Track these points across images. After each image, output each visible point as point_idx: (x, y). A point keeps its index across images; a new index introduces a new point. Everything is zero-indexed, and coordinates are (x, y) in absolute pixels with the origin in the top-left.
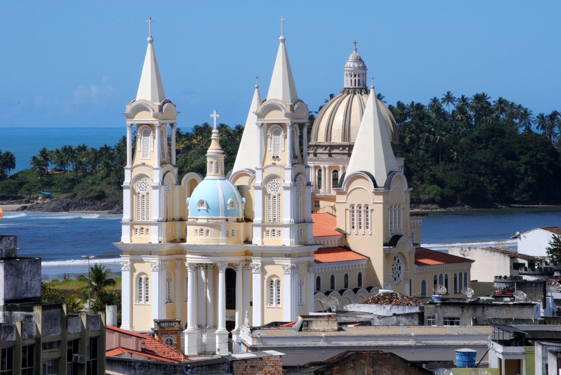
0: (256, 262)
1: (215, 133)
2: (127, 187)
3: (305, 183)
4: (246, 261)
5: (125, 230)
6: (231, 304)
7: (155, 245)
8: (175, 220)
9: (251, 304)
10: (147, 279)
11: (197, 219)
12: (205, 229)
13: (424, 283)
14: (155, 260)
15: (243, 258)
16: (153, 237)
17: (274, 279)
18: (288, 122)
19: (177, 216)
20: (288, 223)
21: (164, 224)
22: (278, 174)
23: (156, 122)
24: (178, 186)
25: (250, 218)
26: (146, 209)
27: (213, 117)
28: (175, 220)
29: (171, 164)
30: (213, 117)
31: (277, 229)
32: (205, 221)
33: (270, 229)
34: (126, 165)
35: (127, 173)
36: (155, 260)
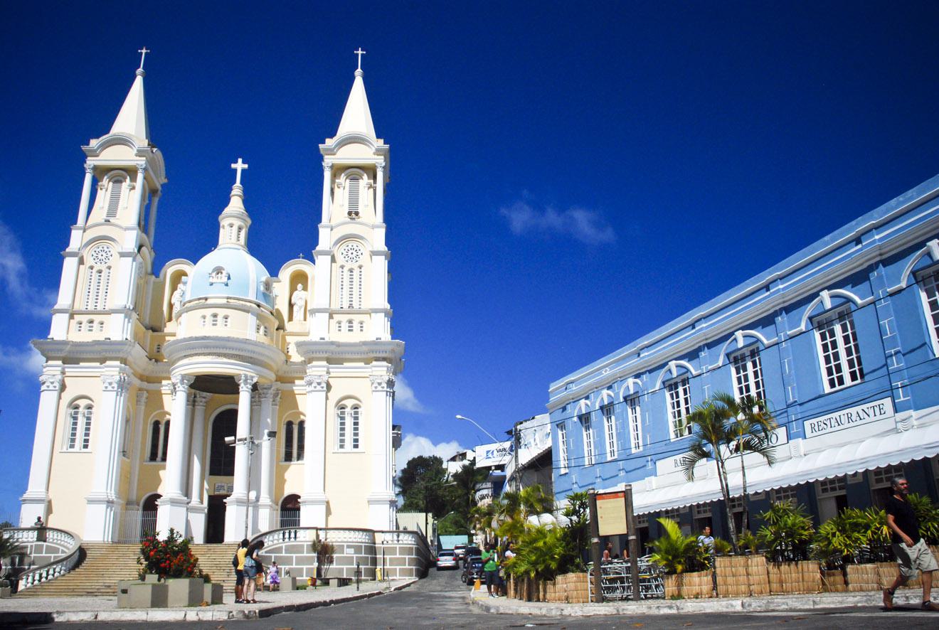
11: (206, 299)
16: (118, 329)
17: (82, 403)
30: (235, 170)
32: (224, 301)
34: (75, 222)
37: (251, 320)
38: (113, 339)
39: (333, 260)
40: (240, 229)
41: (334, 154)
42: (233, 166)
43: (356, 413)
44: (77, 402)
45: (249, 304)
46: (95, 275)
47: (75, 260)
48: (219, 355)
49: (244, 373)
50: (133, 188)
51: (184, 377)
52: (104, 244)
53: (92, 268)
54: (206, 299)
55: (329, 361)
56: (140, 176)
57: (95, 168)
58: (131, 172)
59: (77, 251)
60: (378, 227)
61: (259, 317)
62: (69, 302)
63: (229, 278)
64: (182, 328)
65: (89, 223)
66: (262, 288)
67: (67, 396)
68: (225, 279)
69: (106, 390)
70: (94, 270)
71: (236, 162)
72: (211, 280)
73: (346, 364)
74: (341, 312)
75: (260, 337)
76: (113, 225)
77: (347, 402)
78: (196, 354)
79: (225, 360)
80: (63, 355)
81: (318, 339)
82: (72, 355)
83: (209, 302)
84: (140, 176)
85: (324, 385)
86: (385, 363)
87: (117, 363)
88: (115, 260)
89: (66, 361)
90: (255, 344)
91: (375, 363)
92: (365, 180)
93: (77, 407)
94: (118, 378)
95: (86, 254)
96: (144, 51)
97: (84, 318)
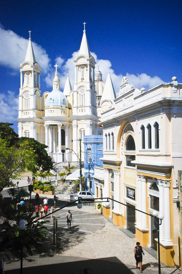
0: (74, 122)
1: (56, 73)
2: (21, 96)
3: (94, 91)
4: (69, 125)
5: (20, 113)
6: (63, 143)
7: (32, 118)
8: (40, 109)
9: (72, 141)
10: (29, 133)
11: (49, 106)
12: (52, 110)
13: (135, 99)
14: (32, 124)
15: (68, 123)
16: (32, 114)
17: (82, 130)
18: (32, 69)
19: (41, 109)
20: (88, 105)
21: (36, 110)
22: (84, 85)
23: (32, 69)
24: (41, 97)
25: (71, 108)
26: (27, 104)
27: (55, 67)
28: (40, 109)
29: (38, 88)
30: (55, 67)
31: (83, 108)
32: (53, 107)
33: (80, 109)
34: (20, 87)
35: (21, 91)
36: (32, 124)
37: (60, 110)
38: (31, 117)
39: (78, 93)
40: (57, 85)
41: (22, 68)
42: (55, 66)
43: (84, 132)
44: (81, 130)
45: (59, 107)
46: (26, 100)
47: (21, 97)
48: (53, 120)
49: (59, 124)
50: (87, 70)
51: (46, 125)
52: (27, 92)
53: (80, 95)
54: (49, 106)
55: (77, 120)
56: (33, 73)
57: (23, 72)
58: (30, 71)
59: (76, 91)
60: (33, 88)
61: (62, 109)
62: (21, 108)
63: (54, 101)
64: (47, 113)
65: (24, 87)
66: (62, 102)
67: (24, 130)
68: (53, 101)
69: (31, 129)
70: (81, 95)
71: (55, 65)
72: (50, 102)
73: (26, 123)
74: (80, 107)
75: (63, 115)
76: (84, 82)
77: (82, 130)
78: (48, 120)
79: (54, 121)
80: (21, 121)
81: (28, 117)
82: (24, 121)
83: (50, 107)
84: (33, 73)
85: (76, 126)
86: (89, 120)
87: (33, 122)
88: (85, 92)
89: (22, 122)
90: (64, 117)
91: (87, 120)
92: (85, 68)
93: (26, 133)
94: (33, 126)
95: (23, 95)
96: (30, 32)
97: (25, 112)
